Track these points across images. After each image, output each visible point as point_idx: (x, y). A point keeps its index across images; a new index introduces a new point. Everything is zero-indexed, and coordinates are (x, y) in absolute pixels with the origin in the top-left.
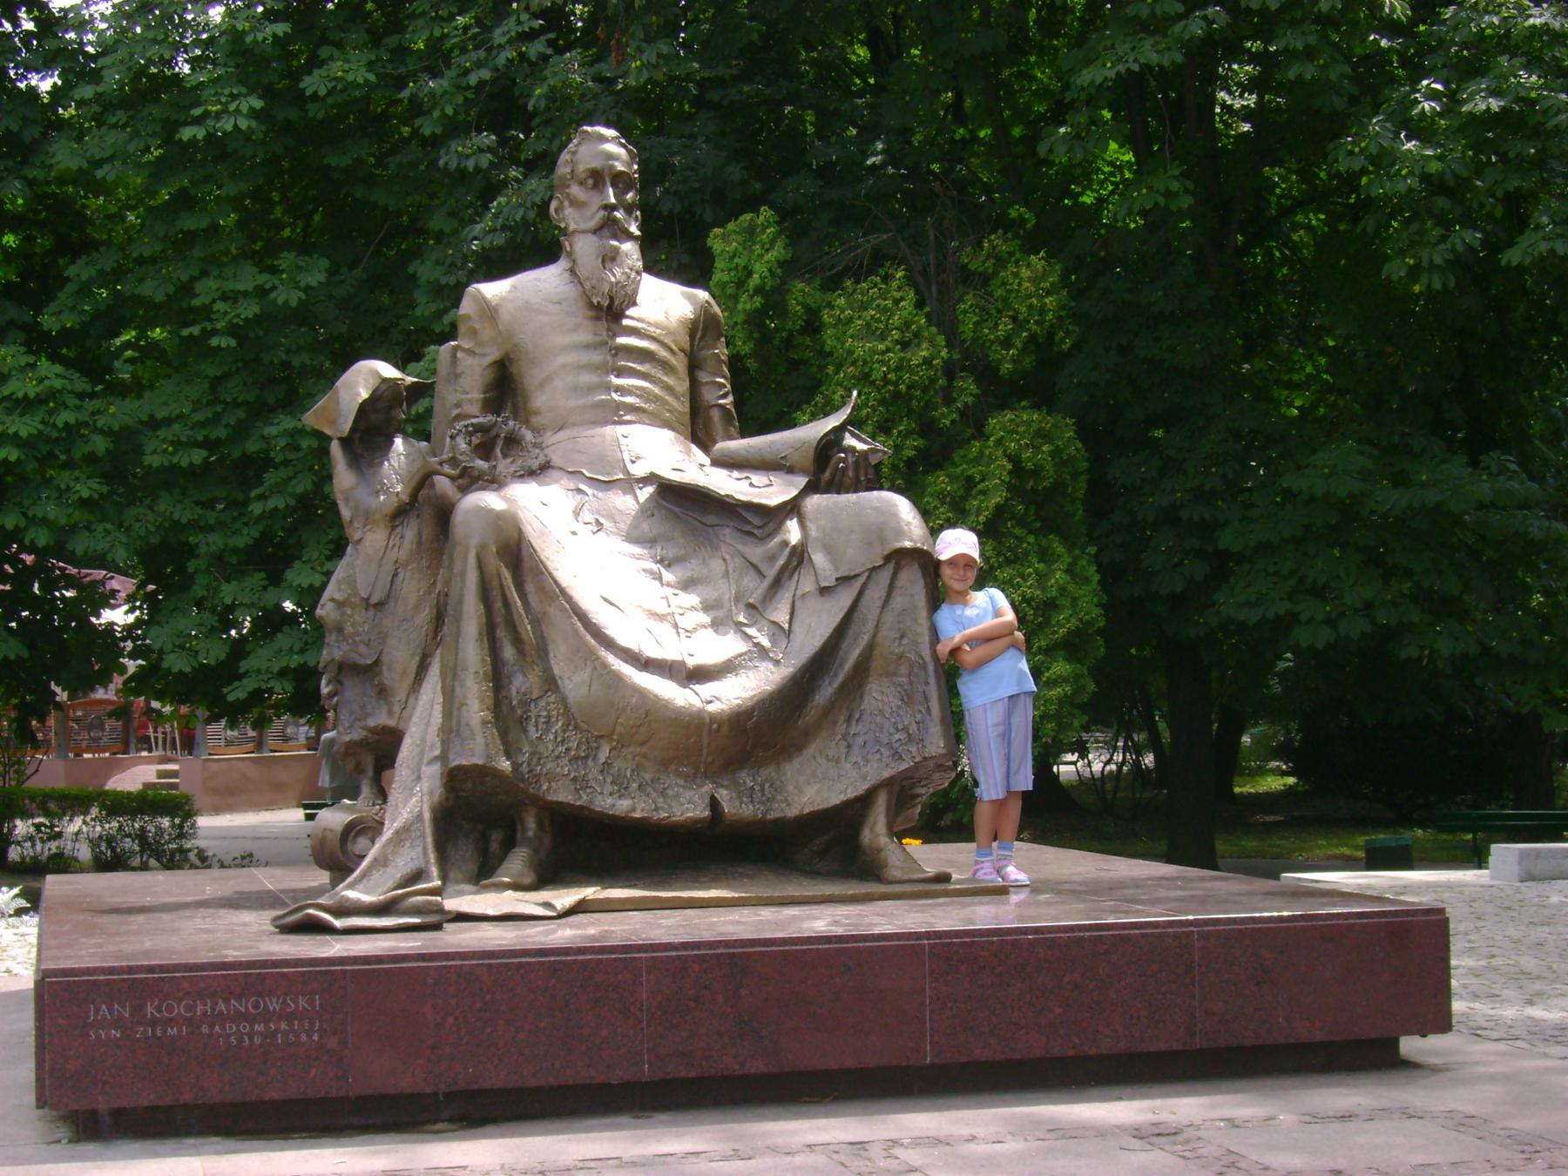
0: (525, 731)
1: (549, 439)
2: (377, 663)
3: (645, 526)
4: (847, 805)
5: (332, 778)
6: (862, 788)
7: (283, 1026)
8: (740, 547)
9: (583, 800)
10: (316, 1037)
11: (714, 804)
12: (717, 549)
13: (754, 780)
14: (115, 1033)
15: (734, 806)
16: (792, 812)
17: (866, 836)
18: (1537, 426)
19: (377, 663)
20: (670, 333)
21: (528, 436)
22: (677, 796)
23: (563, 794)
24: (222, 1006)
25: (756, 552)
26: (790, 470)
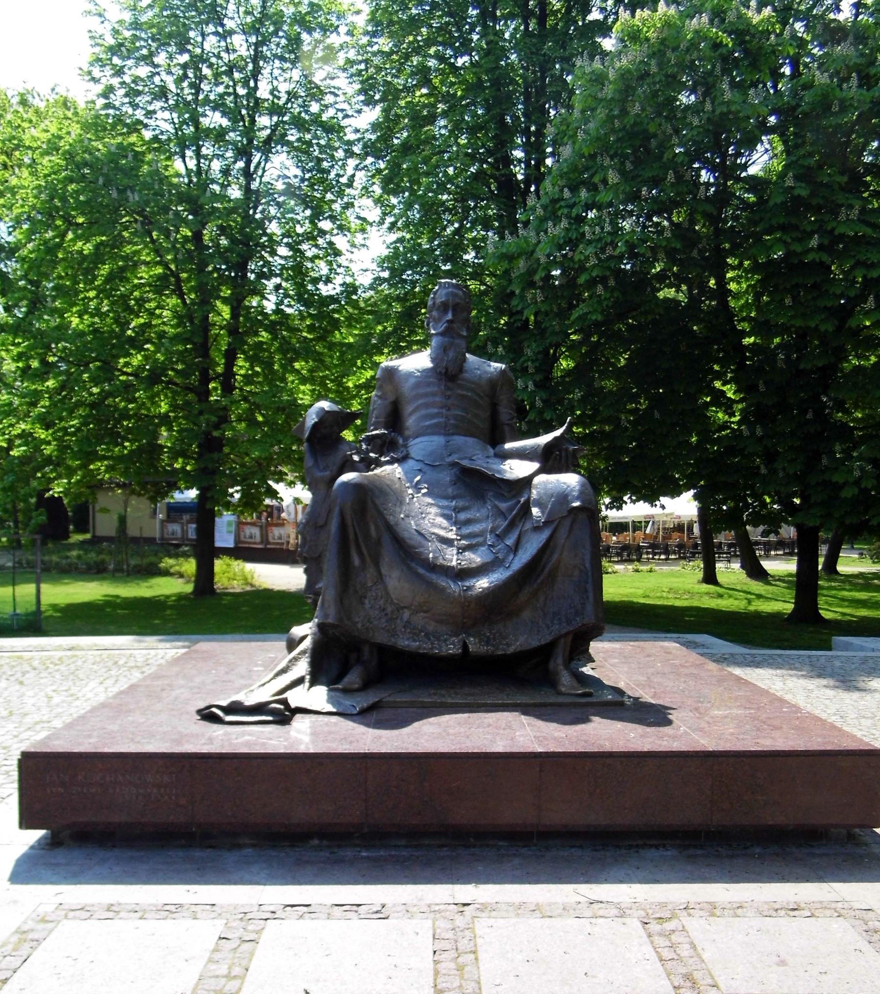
0: (363, 604)
1: (412, 442)
2: (320, 556)
3: (450, 491)
4: (547, 645)
5: (675, 491)
6: (549, 639)
7: (155, 791)
8: (497, 503)
9: (392, 641)
10: (173, 798)
11: (465, 646)
12: (485, 503)
13: (490, 632)
14: (61, 790)
15: (474, 645)
16: (511, 650)
17: (552, 665)
18: (612, 283)
19: (320, 556)
20: (428, 384)
21: (401, 441)
22: (445, 640)
23: (381, 638)
24: (120, 778)
25: (503, 506)
26: (531, 459)
